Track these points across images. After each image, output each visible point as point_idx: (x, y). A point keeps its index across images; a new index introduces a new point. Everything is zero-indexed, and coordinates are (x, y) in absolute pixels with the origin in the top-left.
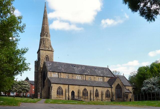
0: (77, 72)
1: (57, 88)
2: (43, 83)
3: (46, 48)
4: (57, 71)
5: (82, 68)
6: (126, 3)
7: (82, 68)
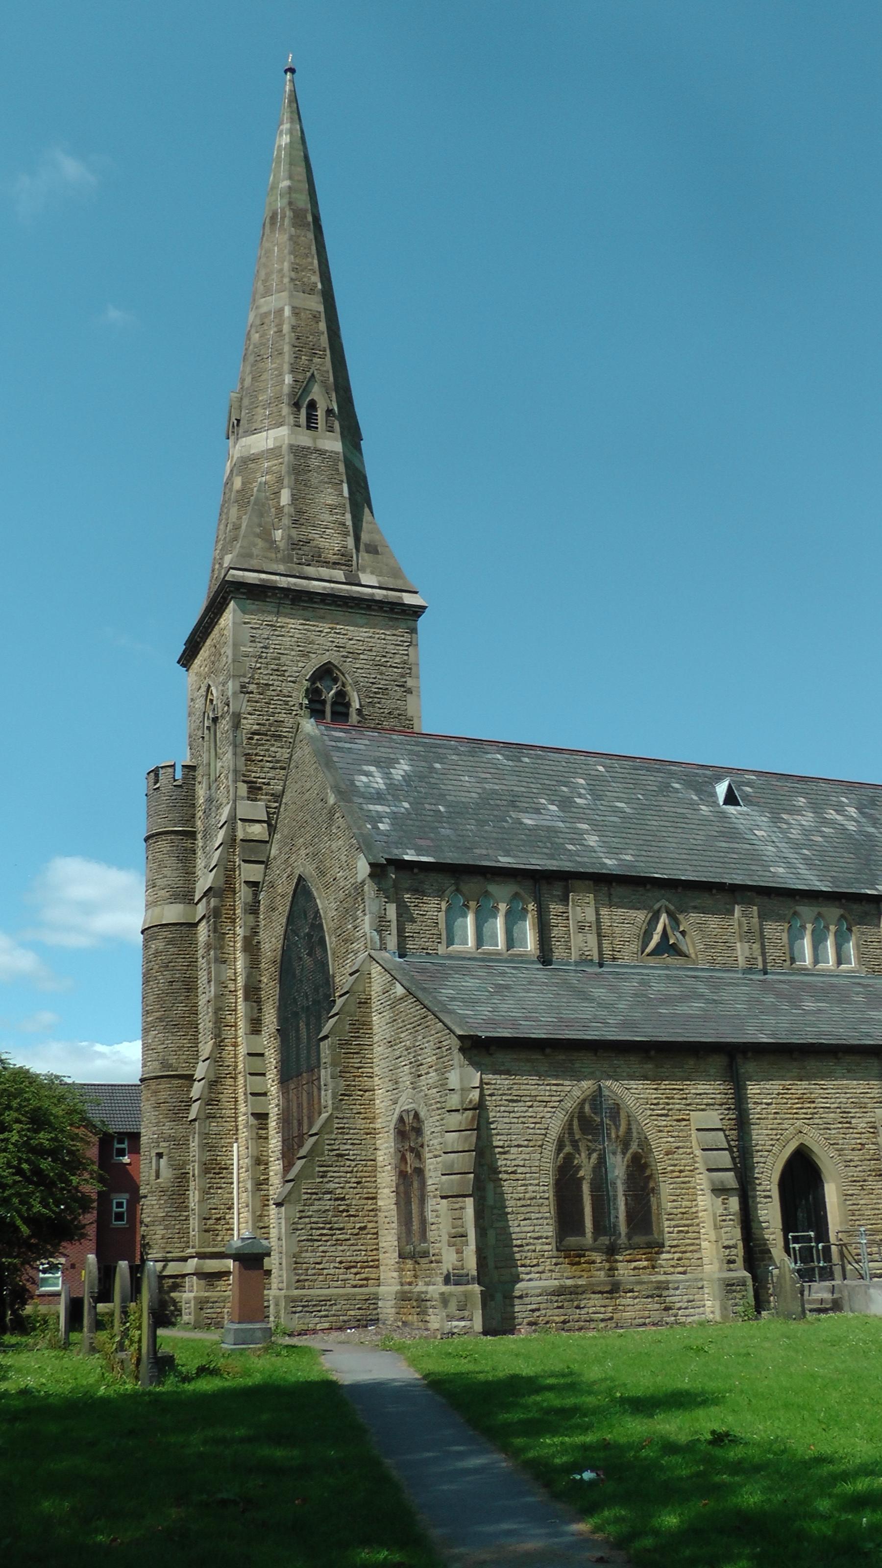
0: (789, 865)
1: (556, 1125)
2: (284, 1079)
3: (311, 571)
4: (505, 861)
5: (832, 814)
6: (645, 1163)
7: (832, 814)
